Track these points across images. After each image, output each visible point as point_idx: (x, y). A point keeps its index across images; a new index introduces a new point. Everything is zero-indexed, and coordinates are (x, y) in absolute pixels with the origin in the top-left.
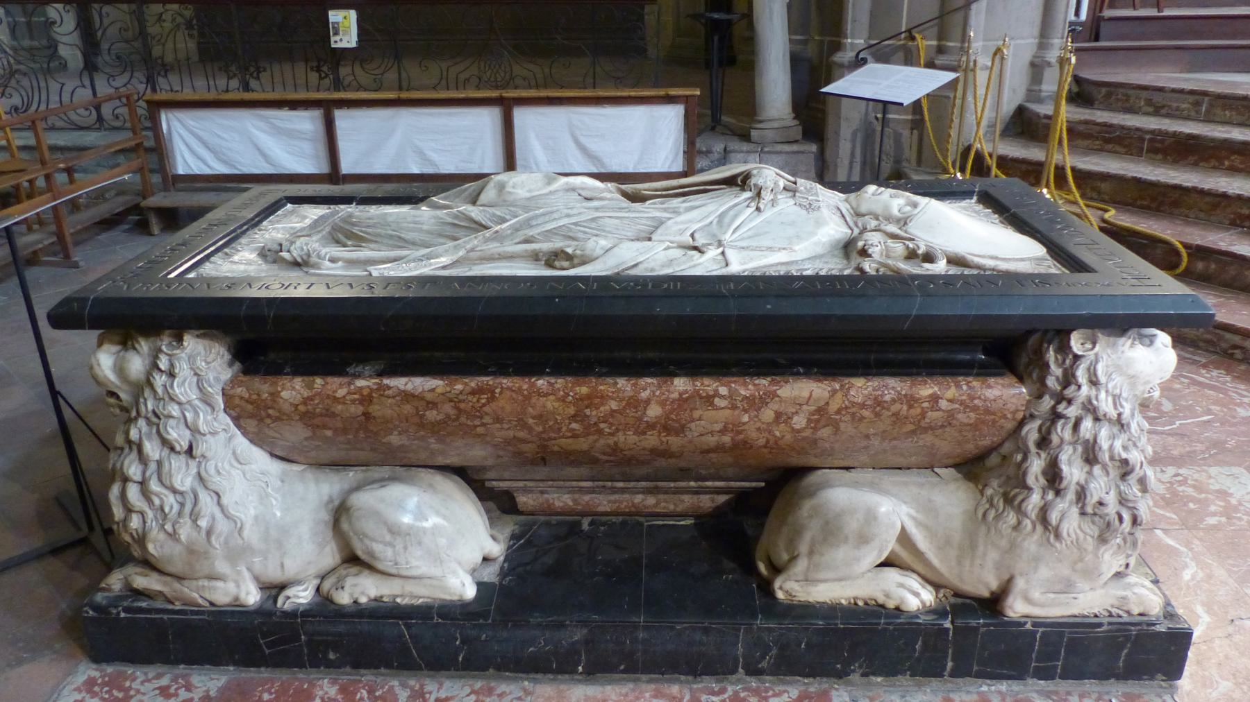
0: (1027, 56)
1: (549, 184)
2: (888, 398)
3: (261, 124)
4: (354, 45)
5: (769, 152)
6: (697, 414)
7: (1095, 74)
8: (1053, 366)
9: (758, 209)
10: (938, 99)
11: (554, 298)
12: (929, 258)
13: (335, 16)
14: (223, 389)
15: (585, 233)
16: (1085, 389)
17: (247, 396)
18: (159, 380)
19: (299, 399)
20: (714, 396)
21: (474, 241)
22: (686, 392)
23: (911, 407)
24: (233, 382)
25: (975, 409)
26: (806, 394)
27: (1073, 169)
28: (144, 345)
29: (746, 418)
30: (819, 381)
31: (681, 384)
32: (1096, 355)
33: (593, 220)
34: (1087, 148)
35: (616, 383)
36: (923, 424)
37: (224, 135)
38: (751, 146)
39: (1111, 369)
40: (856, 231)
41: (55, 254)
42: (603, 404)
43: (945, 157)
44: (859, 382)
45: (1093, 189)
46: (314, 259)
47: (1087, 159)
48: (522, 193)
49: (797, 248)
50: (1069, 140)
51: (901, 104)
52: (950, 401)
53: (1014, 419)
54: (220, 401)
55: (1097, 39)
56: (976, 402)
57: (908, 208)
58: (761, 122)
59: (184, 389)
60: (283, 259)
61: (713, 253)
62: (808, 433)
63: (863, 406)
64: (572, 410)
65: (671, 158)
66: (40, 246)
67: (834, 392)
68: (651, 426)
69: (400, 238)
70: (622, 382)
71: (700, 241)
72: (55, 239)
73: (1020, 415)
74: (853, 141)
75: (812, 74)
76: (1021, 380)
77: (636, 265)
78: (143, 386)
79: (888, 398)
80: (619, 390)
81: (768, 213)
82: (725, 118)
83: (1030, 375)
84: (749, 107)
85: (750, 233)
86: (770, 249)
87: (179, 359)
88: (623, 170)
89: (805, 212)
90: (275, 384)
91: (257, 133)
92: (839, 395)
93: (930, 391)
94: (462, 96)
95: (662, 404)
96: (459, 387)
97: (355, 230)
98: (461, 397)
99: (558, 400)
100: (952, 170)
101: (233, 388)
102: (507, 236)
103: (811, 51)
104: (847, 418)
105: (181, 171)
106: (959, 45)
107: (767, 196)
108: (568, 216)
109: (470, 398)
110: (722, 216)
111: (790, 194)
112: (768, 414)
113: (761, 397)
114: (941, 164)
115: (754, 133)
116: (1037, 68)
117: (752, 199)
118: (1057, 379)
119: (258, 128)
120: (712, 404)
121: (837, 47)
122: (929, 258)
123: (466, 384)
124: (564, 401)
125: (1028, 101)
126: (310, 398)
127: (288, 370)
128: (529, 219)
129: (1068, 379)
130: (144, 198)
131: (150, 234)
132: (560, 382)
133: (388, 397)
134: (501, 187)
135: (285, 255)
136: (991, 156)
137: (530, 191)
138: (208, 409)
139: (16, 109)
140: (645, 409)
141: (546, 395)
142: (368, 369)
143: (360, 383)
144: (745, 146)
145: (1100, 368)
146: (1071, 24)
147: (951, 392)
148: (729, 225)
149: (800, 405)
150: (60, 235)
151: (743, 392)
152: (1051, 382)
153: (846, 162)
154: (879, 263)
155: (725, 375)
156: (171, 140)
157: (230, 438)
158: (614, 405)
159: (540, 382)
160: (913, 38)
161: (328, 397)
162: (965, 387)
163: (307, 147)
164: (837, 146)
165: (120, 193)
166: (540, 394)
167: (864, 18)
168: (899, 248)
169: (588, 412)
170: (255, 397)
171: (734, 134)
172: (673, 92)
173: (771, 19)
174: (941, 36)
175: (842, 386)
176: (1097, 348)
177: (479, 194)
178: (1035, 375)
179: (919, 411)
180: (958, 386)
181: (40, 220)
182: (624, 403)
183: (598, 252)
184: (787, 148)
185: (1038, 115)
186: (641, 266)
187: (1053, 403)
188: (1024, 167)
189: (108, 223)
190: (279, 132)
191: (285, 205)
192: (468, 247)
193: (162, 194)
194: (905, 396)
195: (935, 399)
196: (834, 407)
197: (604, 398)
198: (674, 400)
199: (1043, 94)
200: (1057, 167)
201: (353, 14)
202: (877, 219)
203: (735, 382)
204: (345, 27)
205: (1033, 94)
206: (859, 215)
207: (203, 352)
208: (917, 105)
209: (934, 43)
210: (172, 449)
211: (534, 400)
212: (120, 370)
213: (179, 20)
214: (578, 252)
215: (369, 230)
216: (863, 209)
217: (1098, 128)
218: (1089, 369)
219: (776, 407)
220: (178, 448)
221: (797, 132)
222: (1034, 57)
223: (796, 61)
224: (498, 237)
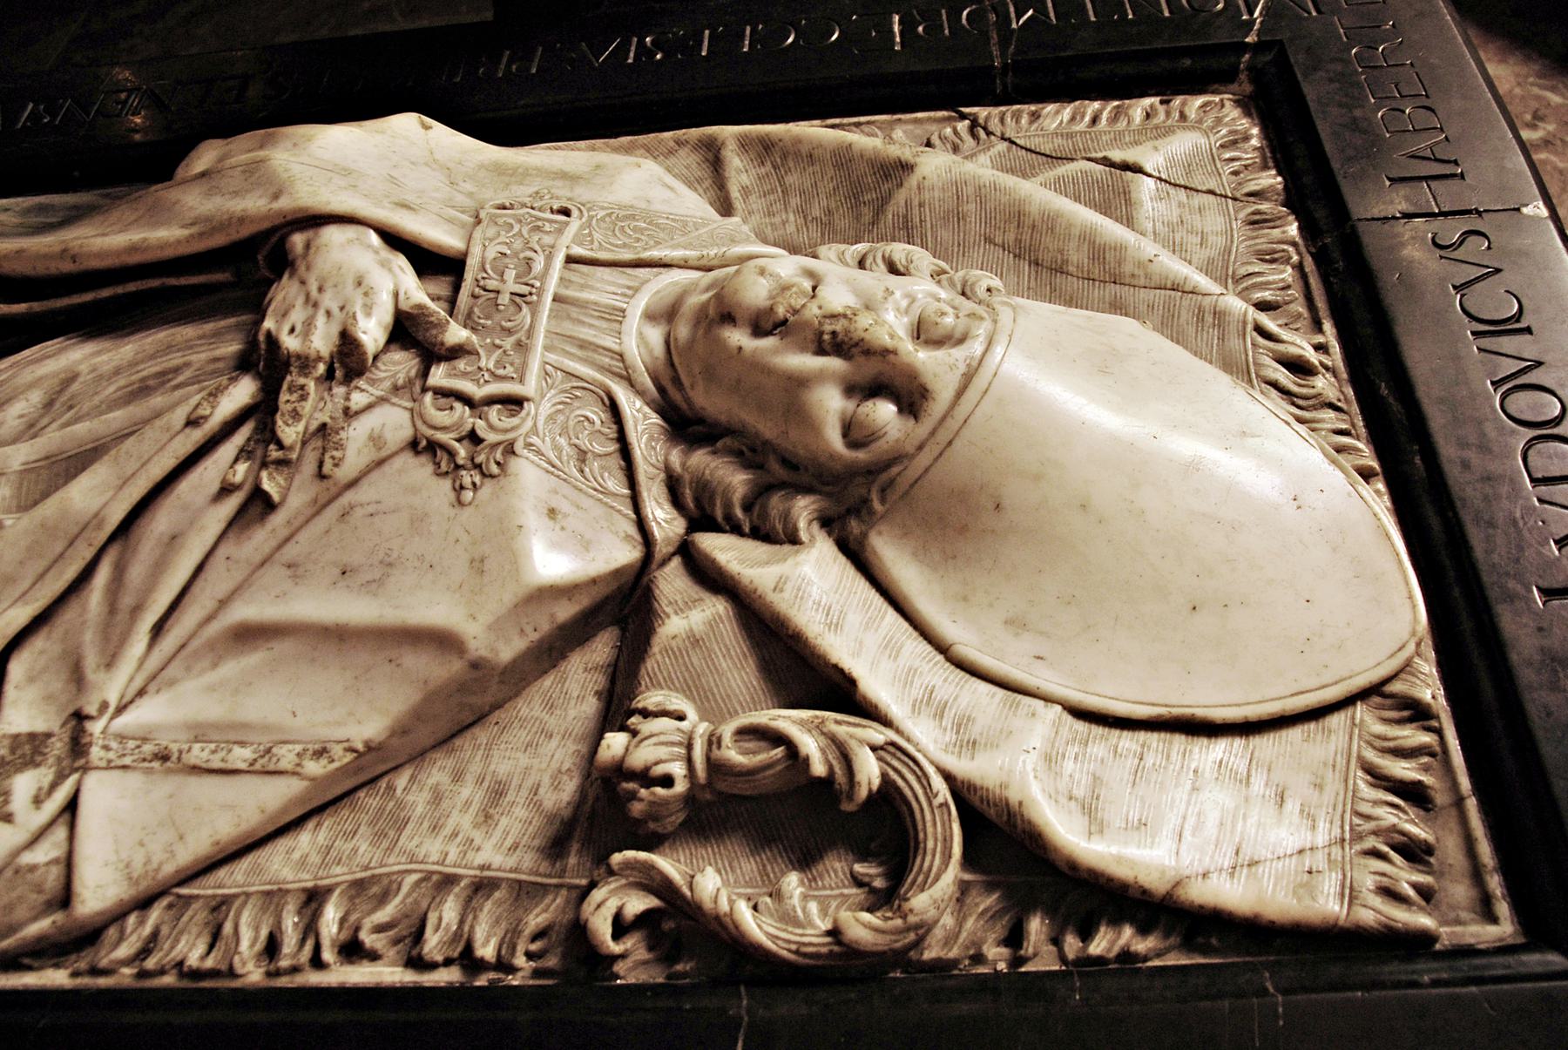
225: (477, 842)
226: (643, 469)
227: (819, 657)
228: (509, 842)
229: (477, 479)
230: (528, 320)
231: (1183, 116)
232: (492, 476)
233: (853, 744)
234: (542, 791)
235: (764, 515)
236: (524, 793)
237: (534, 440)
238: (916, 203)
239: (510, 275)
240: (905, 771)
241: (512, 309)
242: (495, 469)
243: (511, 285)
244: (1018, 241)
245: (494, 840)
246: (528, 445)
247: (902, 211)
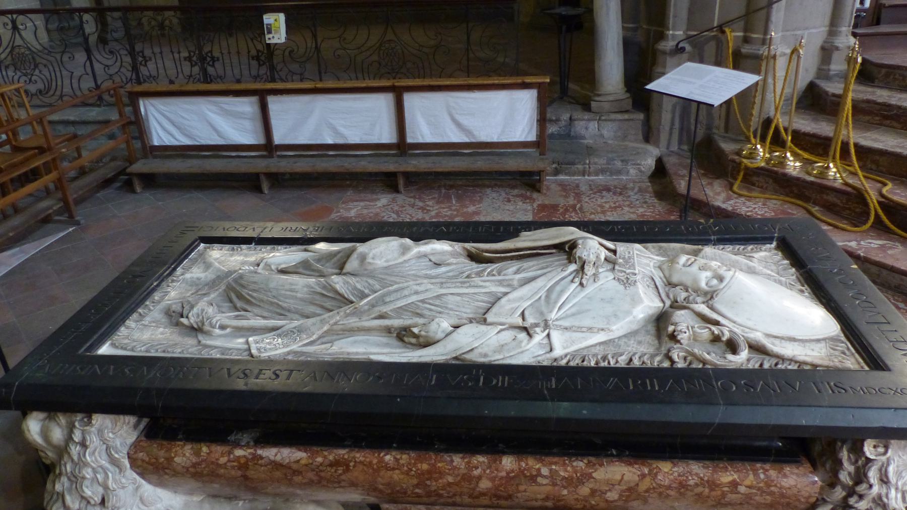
0: (818, 41)
1: (403, 254)
2: (691, 482)
3: (214, 108)
4: (283, 40)
5: (605, 120)
6: (522, 488)
7: (877, 56)
8: (846, 464)
9: (581, 284)
10: (745, 97)
11: (396, 397)
12: (732, 346)
13: (268, 19)
14: (128, 454)
15: (431, 310)
16: (876, 489)
17: (147, 459)
18: (75, 450)
19: (189, 464)
20: (536, 476)
21: (338, 317)
22: (513, 471)
23: (712, 490)
24: (136, 446)
25: (772, 494)
26: (618, 477)
27: (856, 145)
28: (62, 419)
29: (565, 492)
30: (630, 464)
31: (508, 462)
32: (888, 460)
33: (439, 297)
34: (868, 122)
35: (452, 461)
36: (723, 501)
37: (186, 116)
38: (591, 115)
39: (901, 469)
40: (668, 303)
41: (61, 215)
42: (441, 478)
43: (749, 131)
44: (665, 467)
45: (873, 162)
46: (207, 328)
47: (868, 134)
48: (380, 263)
49: (614, 328)
50: (853, 115)
51: (713, 106)
52: (749, 487)
53: (807, 502)
54: (126, 462)
55: (878, 22)
56: (772, 488)
57: (715, 282)
58: (599, 95)
59: (96, 457)
60: (183, 325)
61: (539, 336)
62: (620, 503)
63: (669, 487)
64: (415, 481)
65: (527, 130)
66: (51, 211)
67: (643, 476)
68: (483, 494)
69: (278, 305)
70: (458, 460)
71: (530, 320)
72: (62, 204)
73: (813, 500)
74: (673, 112)
75: (642, 63)
76: (815, 467)
77: (472, 350)
78: (62, 451)
79: (691, 482)
80: (455, 467)
81: (590, 289)
82: (572, 86)
83: (824, 465)
84: (589, 75)
85: (573, 310)
86: (590, 329)
87: (89, 433)
88: (489, 140)
89: (622, 287)
90: (169, 450)
91: (210, 114)
92: (648, 479)
93: (730, 479)
94: (364, 85)
95: (493, 479)
96: (320, 459)
97: (244, 292)
98: (321, 468)
99: (403, 473)
100: (753, 141)
101: (136, 452)
102: (365, 312)
103: (640, 37)
104: (655, 495)
105: (156, 143)
106: (762, 36)
107: (589, 270)
108: (417, 293)
109: (329, 469)
110: (550, 291)
111: (610, 266)
112: (585, 490)
113: (578, 478)
114: (744, 133)
115: (593, 104)
116: (827, 52)
117: (577, 271)
118: (850, 474)
119: (210, 110)
120: (535, 481)
121: (661, 36)
122: (732, 346)
123: (325, 457)
124: (408, 474)
125: (818, 78)
126: (199, 464)
127: (180, 436)
128: (384, 295)
129: (860, 477)
130: (131, 164)
131: (133, 191)
132: (404, 458)
133: (261, 466)
134: (363, 258)
135: (184, 321)
136: (786, 130)
137: (387, 261)
138: (117, 469)
139: (40, 91)
140: (477, 483)
141: (394, 469)
142: (245, 438)
143: (239, 452)
144: (587, 116)
145: (891, 469)
146: (858, 10)
147: (750, 479)
148: (556, 302)
149: (613, 485)
150: (65, 200)
151: (562, 473)
152: (844, 477)
153: (667, 128)
154: (687, 351)
155: (547, 455)
156: (148, 120)
157: (137, 489)
158: (450, 479)
159: (388, 457)
160: (723, 32)
161: (212, 463)
162: (762, 476)
163: (248, 124)
164: (660, 117)
165: (113, 159)
166: (388, 468)
167: (684, 14)
168: (705, 333)
169: (428, 483)
170: (154, 460)
171: (578, 103)
172: (528, 80)
173: (608, 14)
174: (746, 30)
175: (650, 470)
176: (890, 452)
177: (344, 263)
178: (828, 466)
179: (719, 493)
180: (755, 472)
181: (48, 192)
182: (459, 478)
183: (440, 335)
184: (619, 116)
185: (826, 93)
186: (475, 351)
187: (844, 494)
188: (814, 140)
189: (107, 183)
190: (227, 113)
191: (198, 245)
192: (332, 322)
193: (143, 161)
194: (708, 481)
195: (734, 484)
196: (643, 487)
197: (441, 474)
198: (502, 478)
199: (832, 73)
200: (842, 143)
201: (282, 17)
202: (687, 291)
203: (555, 463)
204: (277, 27)
205: (823, 72)
206: (670, 284)
207: (110, 425)
208: (728, 102)
209: (741, 34)
210: (89, 502)
211: (382, 473)
212: (45, 434)
213: (153, 23)
214: (423, 333)
215: (255, 294)
216: (675, 279)
217: (878, 107)
218: (880, 470)
219: (591, 486)
220: (92, 502)
221: (628, 104)
222: (825, 42)
223: (627, 45)
224: (358, 313)
226: (661, 291)
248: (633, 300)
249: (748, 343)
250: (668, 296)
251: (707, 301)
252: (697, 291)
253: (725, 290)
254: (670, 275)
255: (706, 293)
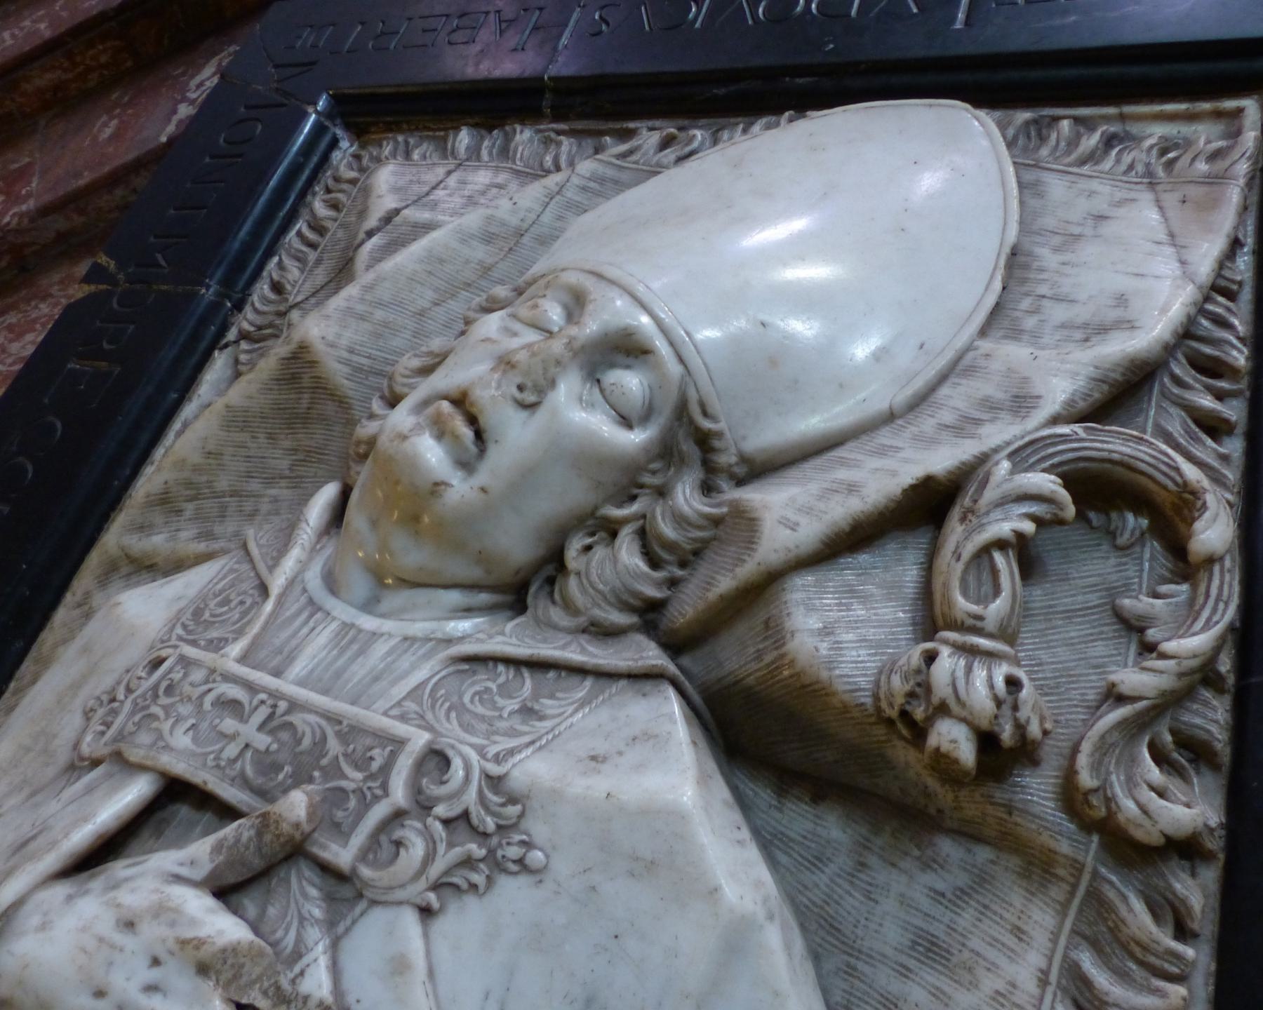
57: (630, 382)
89: (512, 893)
111: (304, 894)
202: (611, 530)
216: (515, 544)
225: (1000, 985)
226: (573, 655)
227: (892, 505)
228: (1010, 940)
229: (517, 837)
230: (312, 718)
231: (353, 182)
232: (521, 816)
233: (1007, 487)
234: (940, 886)
235: (671, 546)
236: (937, 911)
237: (492, 750)
238: (345, 355)
239: (229, 724)
240: (1051, 450)
241: (285, 736)
242: (513, 810)
243: (250, 731)
244: (436, 290)
245: (1002, 961)
246: (497, 759)
247: (346, 370)
248: (644, 867)
249: (1081, 419)
250: (603, 632)
251: (709, 467)
252: (630, 480)
253: (695, 362)
254: (482, 558)
255: (666, 453)
